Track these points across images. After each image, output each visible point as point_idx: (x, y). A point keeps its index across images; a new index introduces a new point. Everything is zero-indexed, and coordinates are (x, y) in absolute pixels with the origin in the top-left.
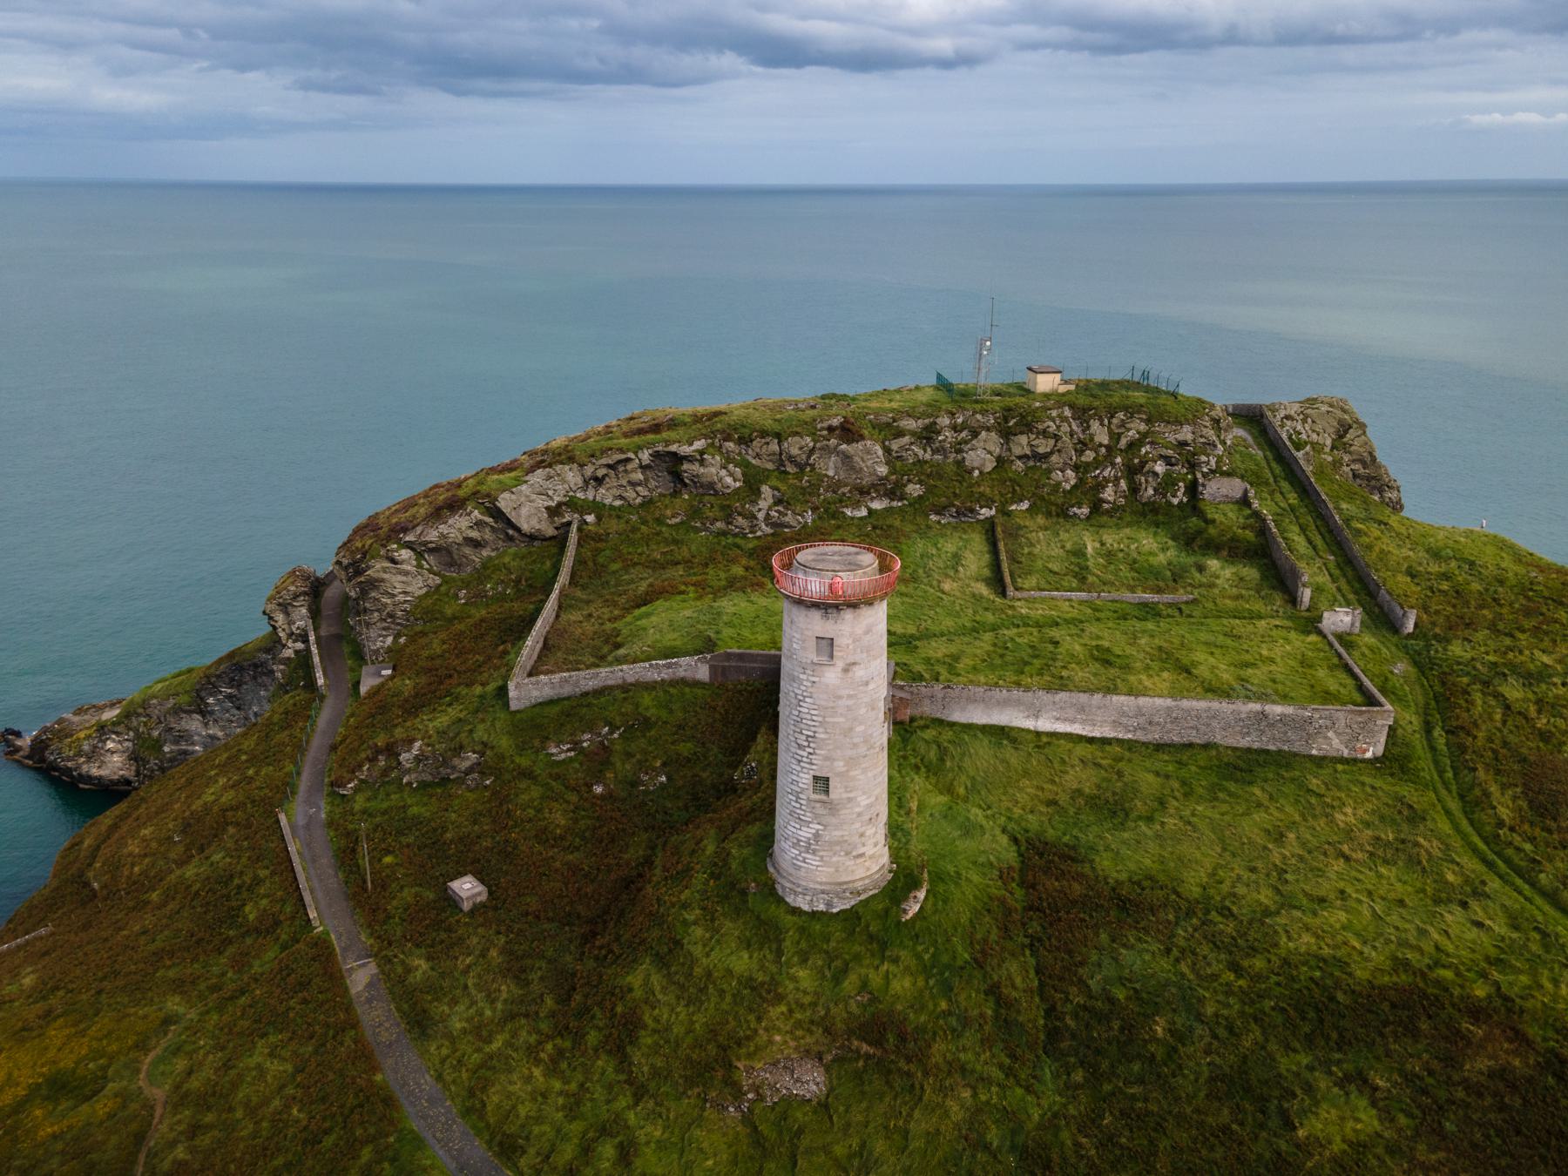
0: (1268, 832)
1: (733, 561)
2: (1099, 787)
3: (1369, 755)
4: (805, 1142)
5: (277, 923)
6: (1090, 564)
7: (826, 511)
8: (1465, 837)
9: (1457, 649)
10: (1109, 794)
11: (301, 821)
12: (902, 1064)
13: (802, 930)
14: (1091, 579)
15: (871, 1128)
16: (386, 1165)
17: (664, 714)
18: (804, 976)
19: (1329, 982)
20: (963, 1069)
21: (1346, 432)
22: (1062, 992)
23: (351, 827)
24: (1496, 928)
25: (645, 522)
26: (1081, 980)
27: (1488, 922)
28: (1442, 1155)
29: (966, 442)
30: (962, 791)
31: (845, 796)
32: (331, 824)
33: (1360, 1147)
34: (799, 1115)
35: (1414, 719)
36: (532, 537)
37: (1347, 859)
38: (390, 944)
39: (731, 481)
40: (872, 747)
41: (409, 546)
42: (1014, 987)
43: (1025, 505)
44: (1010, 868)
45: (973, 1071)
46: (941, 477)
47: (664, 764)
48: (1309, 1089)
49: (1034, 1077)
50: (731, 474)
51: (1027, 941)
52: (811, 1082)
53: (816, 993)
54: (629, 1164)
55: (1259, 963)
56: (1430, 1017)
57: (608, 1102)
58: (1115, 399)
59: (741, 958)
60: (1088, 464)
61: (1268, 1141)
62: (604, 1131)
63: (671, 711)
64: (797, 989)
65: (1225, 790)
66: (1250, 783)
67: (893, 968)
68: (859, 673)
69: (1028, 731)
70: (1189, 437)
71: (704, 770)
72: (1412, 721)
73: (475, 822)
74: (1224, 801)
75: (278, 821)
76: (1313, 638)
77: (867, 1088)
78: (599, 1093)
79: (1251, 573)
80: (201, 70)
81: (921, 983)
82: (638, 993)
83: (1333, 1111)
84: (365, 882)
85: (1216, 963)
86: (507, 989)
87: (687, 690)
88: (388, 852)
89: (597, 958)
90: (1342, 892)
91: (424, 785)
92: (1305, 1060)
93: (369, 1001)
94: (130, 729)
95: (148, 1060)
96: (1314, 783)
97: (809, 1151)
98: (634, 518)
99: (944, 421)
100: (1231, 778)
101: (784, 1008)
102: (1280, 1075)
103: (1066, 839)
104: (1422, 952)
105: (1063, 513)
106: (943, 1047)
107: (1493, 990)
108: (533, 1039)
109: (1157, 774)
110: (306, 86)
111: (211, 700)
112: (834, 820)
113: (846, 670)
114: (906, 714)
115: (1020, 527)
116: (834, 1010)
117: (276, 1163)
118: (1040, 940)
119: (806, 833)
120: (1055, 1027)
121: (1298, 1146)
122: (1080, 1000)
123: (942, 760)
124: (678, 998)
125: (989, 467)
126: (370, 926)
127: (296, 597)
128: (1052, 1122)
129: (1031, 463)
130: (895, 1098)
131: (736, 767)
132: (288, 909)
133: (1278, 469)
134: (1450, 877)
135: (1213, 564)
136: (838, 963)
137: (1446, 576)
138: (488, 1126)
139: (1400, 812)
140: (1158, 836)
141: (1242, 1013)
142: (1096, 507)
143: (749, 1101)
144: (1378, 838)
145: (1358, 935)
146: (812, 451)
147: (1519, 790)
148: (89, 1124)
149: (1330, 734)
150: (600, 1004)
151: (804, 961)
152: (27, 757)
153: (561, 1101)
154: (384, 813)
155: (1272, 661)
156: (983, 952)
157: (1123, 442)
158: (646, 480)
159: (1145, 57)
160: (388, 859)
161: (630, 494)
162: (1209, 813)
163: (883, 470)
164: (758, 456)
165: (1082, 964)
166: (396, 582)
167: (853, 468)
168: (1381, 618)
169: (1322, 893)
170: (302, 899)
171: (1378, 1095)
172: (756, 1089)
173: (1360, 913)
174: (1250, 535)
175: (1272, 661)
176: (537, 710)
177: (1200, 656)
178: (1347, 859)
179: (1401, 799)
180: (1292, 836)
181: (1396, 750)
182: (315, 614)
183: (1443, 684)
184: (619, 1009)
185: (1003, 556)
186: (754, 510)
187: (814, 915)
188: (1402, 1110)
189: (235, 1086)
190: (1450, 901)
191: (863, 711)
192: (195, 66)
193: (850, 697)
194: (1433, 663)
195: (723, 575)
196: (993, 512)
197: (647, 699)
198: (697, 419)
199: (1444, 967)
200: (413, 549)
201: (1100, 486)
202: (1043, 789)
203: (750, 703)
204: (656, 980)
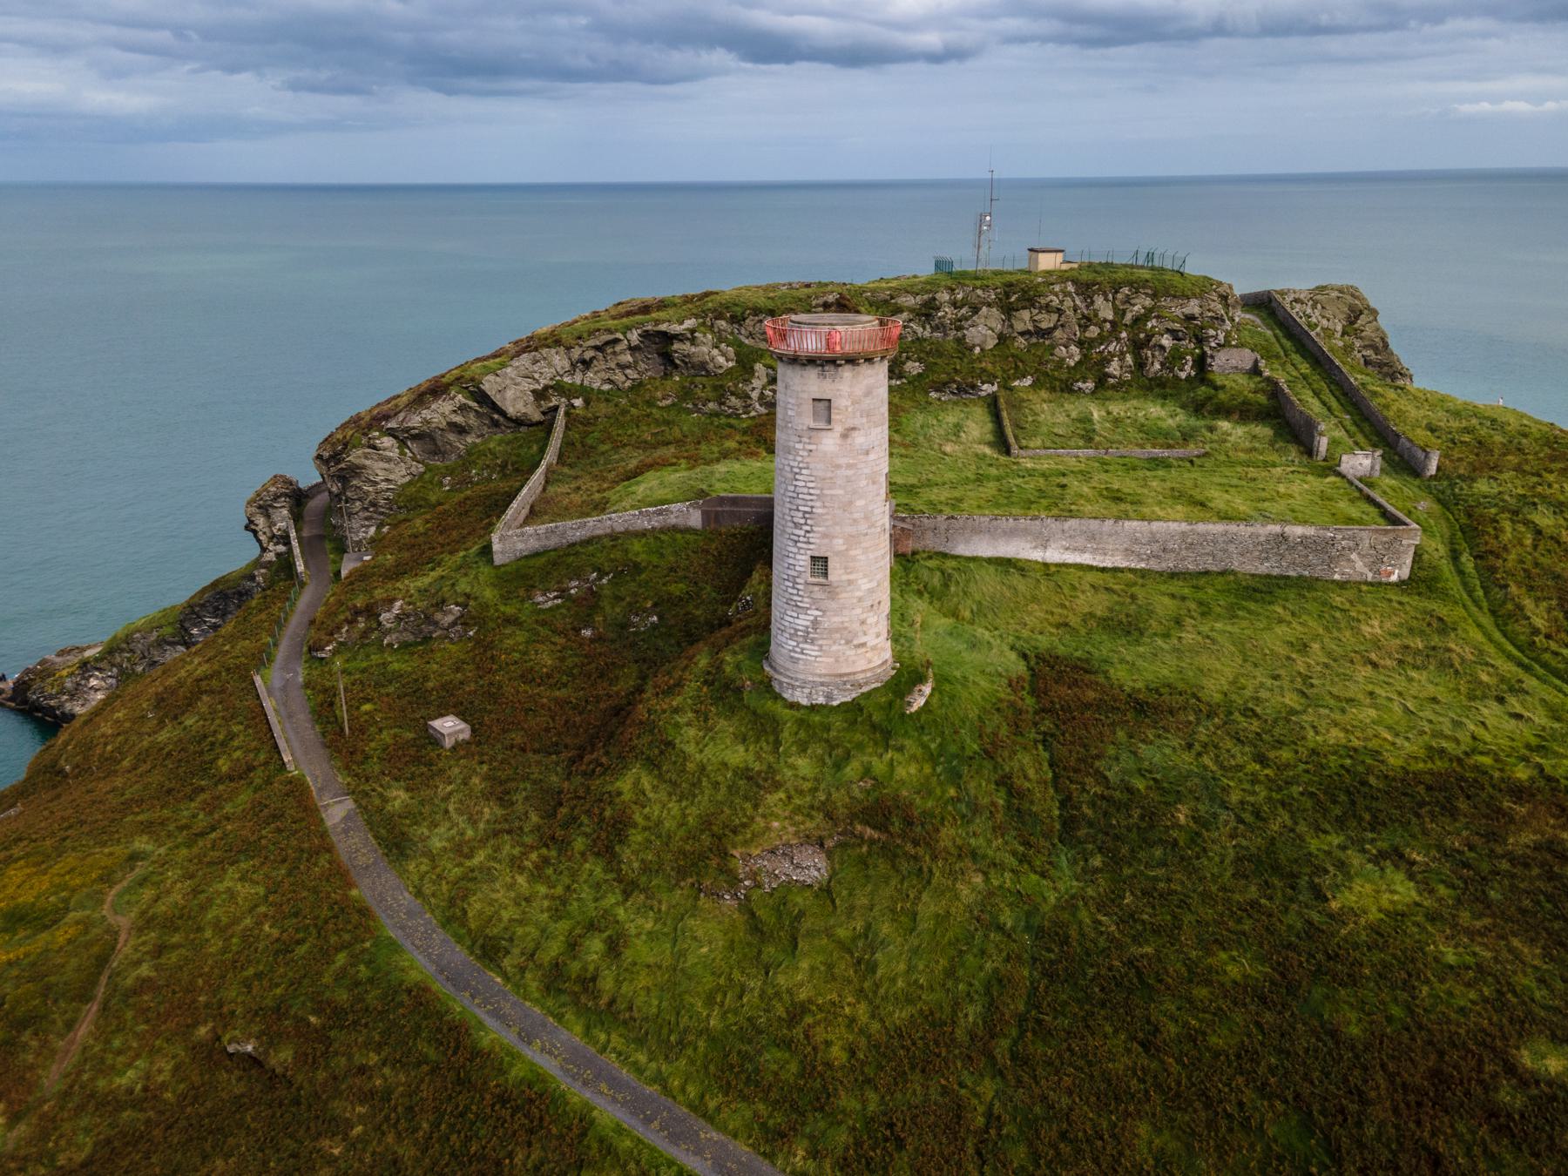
1: (727, 437)
2: (1111, 610)
3: (1394, 578)
4: (807, 924)
5: (251, 768)
6: (1097, 427)
8: (1498, 646)
9: (1482, 486)
10: (1123, 617)
11: (277, 684)
12: (909, 847)
13: (801, 722)
14: (1097, 439)
16: (362, 967)
17: (655, 559)
18: (804, 765)
19: (1361, 769)
20: (974, 855)
21: (1357, 318)
23: (328, 684)
24: (1536, 720)
25: (634, 405)
26: (1097, 771)
27: (1526, 714)
28: (1487, 921)
29: (967, 319)
30: (967, 614)
31: (845, 577)
32: (307, 685)
33: (1398, 916)
34: (799, 900)
35: (1440, 547)
36: (518, 422)
37: (1375, 665)
38: (367, 780)
39: (723, 360)
40: (872, 526)
41: (391, 433)
42: (1026, 777)
43: (1028, 381)
44: (1020, 678)
45: (984, 857)
46: (940, 355)
47: (655, 605)
48: (1342, 865)
49: (1050, 863)
50: (723, 354)
51: (1040, 737)
52: (813, 867)
53: (816, 779)
54: (618, 955)
55: (1286, 755)
56: (1468, 797)
57: (596, 900)
58: (1120, 275)
60: (1092, 340)
61: (1299, 914)
62: (592, 927)
63: (662, 556)
64: (796, 776)
65: (1244, 608)
67: (897, 756)
68: (859, 439)
69: (1037, 562)
70: (1197, 311)
71: (697, 607)
72: (1437, 550)
73: (458, 670)
74: (1244, 618)
75: (253, 683)
76: (1332, 479)
77: (871, 872)
78: (587, 893)
79: (1264, 431)
80: (194, 71)
81: (927, 769)
82: (627, 797)
83: (1368, 886)
84: (342, 729)
85: (1240, 755)
86: (489, 811)
87: (679, 536)
88: (367, 700)
89: (584, 774)
91: (405, 646)
92: (1336, 840)
93: (346, 831)
94: (113, 665)
95: (113, 892)
96: (1338, 600)
97: (810, 934)
98: (624, 401)
99: (944, 296)
100: (1250, 598)
101: (782, 795)
102: (1310, 854)
103: (1078, 654)
104: (1457, 741)
105: (1067, 388)
106: (952, 832)
107: (1535, 772)
108: (516, 851)
109: (1173, 596)
110: (295, 86)
111: (195, 631)
112: (833, 605)
113: (845, 436)
114: (909, 546)
115: (1023, 400)
116: (835, 795)
117: (245, 973)
118: (1052, 735)
119: (803, 621)
121: (1331, 916)
122: (1098, 790)
123: (946, 586)
124: (670, 794)
125: (991, 344)
126: (347, 768)
127: (276, 498)
128: (1070, 904)
129: (1034, 340)
131: (730, 605)
132: (262, 757)
133: (1288, 344)
134: (1485, 678)
135: (1224, 425)
137: (1467, 430)
138: (470, 930)
139: (1429, 625)
140: (1175, 650)
141: (1270, 799)
142: (1102, 381)
143: (746, 888)
144: (1407, 647)
145: (1389, 728)
147: (1554, 602)
148: (47, 950)
149: (1354, 556)
150: (588, 813)
152: (11, 699)
153: (546, 903)
154: (364, 671)
155: (1291, 496)
156: (993, 743)
157: (1128, 317)
158: (636, 362)
159: (1131, 50)
160: (367, 707)
161: (619, 377)
162: (1229, 628)
164: (751, 335)
165: (1098, 757)
166: (378, 469)
168: (1402, 461)
169: (1350, 694)
170: (276, 747)
172: (754, 875)
173: (1391, 710)
174: (1262, 399)
175: (1291, 496)
176: (522, 562)
177: (1214, 493)
178: (1375, 665)
180: (1316, 646)
181: (1422, 574)
182: (297, 517)
183: (1470, 516)
184: (608, 813)
185: (1006, 422)
186: (748, 389)
187: (813, 708)
188: (1443, 882)
189: (203, 908)
190: (1485, 697)
191: (863, 483)
192: (187, 67)
193: (849, 466)
194: (1457, 499)
195: (715, 449)
196: (995, 388)
197: (637, 546)
198: (688, 300)
199: (1481, 753)
200: (395, 437)
201: (1106, 361)
202: (1052, 613)
203: (744, 546)
204: (646, 782)
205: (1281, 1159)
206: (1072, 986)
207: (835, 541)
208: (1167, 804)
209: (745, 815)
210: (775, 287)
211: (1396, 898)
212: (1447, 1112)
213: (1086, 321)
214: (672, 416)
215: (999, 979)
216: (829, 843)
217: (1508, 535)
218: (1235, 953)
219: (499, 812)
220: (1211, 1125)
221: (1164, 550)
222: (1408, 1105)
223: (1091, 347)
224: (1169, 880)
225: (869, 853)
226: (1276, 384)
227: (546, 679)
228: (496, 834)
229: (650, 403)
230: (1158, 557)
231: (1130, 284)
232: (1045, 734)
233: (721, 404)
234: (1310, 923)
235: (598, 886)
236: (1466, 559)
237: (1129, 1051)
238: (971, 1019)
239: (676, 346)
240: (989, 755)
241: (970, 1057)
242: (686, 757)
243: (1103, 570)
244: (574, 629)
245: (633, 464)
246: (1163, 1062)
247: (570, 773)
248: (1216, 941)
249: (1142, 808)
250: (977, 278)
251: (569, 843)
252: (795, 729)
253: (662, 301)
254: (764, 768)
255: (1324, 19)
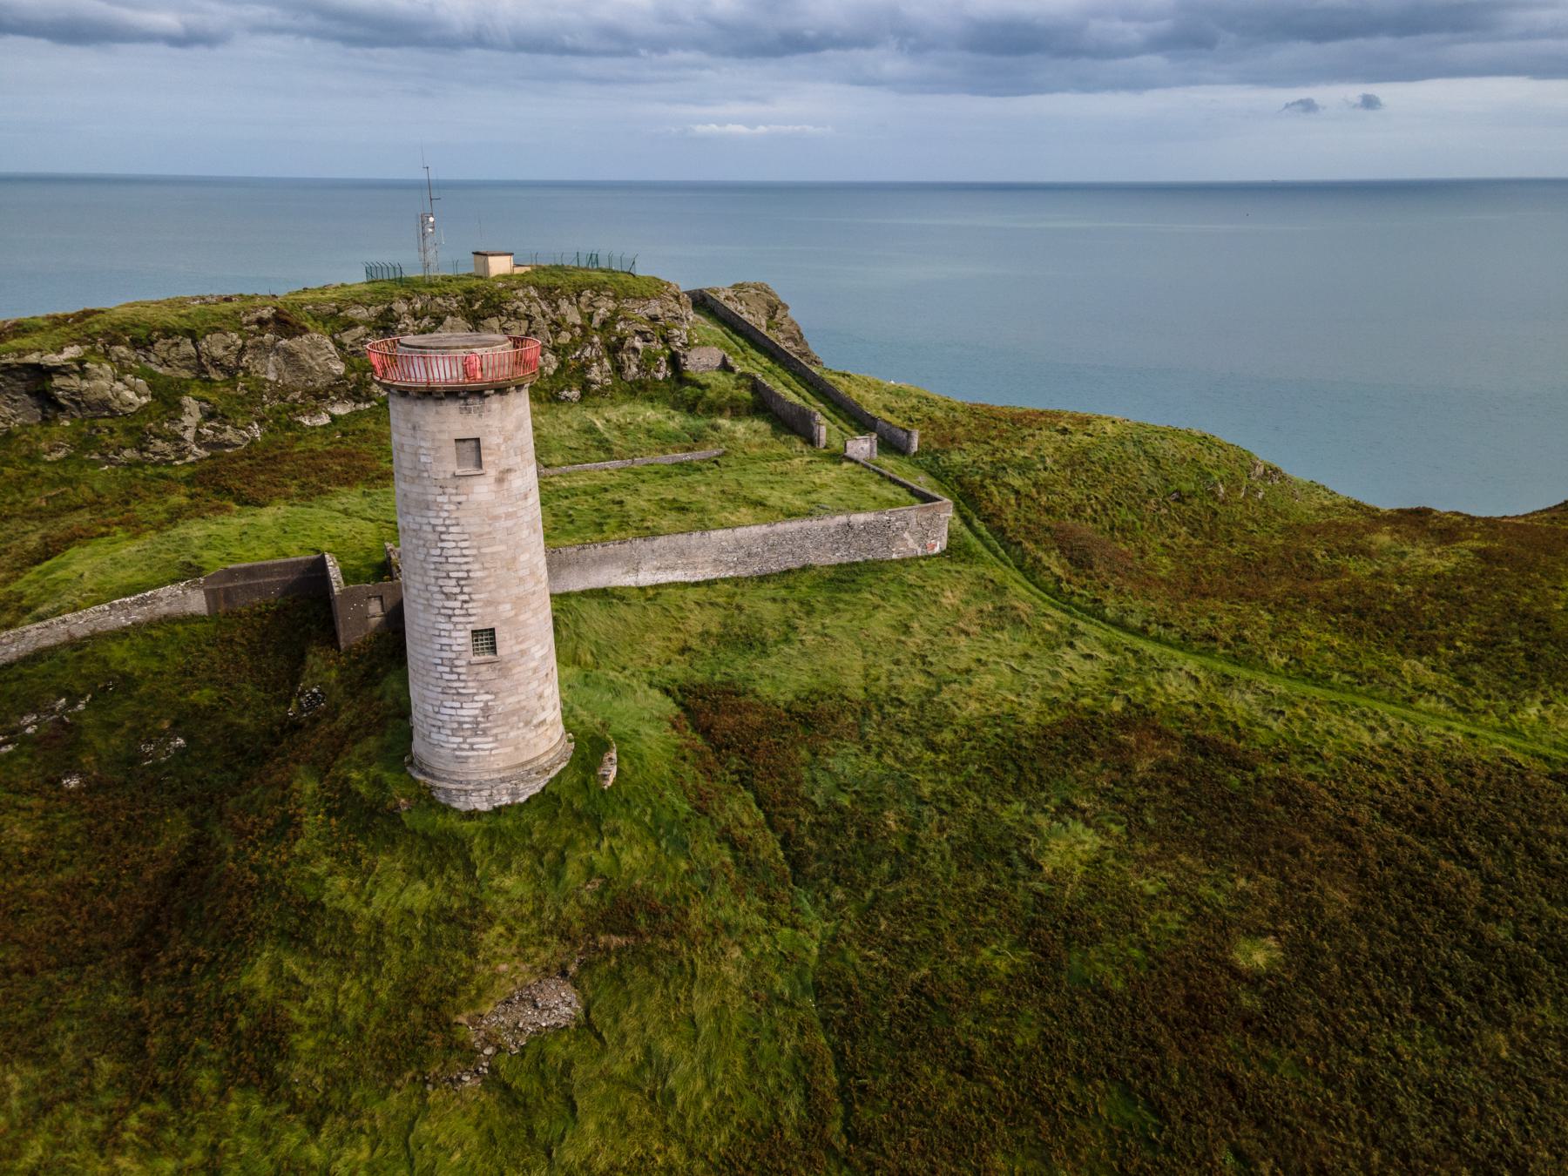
0: (893, 627)
1: (171, 492)
3: (937, 550)
4: (578, 1073)
7: (277, 422)
9: (957, 458)
10: (737, 630)
12: (663, 944)
13: (491, 833)
15: (650, 1031)
17: (154, 664)
20: (727, 927)
22: (791, 816)
26: (804, 799)
31: (516, 648)
34: (558, 1048)
39: (133, 396)
42: (742, 825)
45: (737, 927)
47: (176, 724)
48: (1034, 829)
49: (797, 911)
51: (736, 777)
52: (561, 1004)
55: (947, 736)
57: (267, 1150)
59: (418, 891)
60: (566, 346)
63: (163, 657)
64: (510, 901)
65: (841, 600)
66: (859, 591)
69: (630, 587)
70: (659, 311)
71: (241, 716)
77: (630, 986)
79: (761, 425)
81: (652, 848)
87: (179, 628)
90: (979, 660)
96: (911, 579)
99: (401, 307)
103: (718, 677)
108: (98, 1124)
109: (774, 600)
112: (506, 684)
113: (500, 480)
116: (565, 910)
119: (470, 711)
120: (799, 854)
121: (1050, 882)
122: (810, 818)
124: (339, 972)
130: (666, 985)
134: (1048, 627)
136: (549, 856)
141: (955, 783)
145: (1011, 690)
146: (242, 351)
149: (906, 535)
150: (206, 1033)
151: (506, 868)
157: (596, 322)
162: (836, 622)
163: (339, 368)
164: (165, 362)
165: (798, 782)
167: (301, 368)
169: (963, 666)
171: (1088, 815)
174: (747, 395)
178: (967, 634)
179: (981, 577)
180: (916, 625)
181: (955, 542)
184: (242, 1023)
186: (178, 428)
187: (498, 811)
188: (1112, 821)
191: (525, 533)
193: (508, 516)
198: (58, 322)
201: (585, 367)
205: (1122, 1136)
206: (869, 1032)
207: (501, 608)
208: (875, 813)
209: (461, 969)
210: (182, 303)
211: (1087, 847)
212: (1215, 1033)
213: (557, 326)
214: (71, 472)
215: (805, 1058)
216: (572, 969)
217: (997, 499)
218: (994, 947)
219: (34, 1074)
220: (1055, 1129)
221: (749, 555)
222: (1187, 1038)
223: (566, 354)
224: (909, 892)
225: (619, 964)
226: (754, 378)
227: (31, 861)
228: (46, 1108)
229: (32, 458)
230: (744, 563)
231: (591, 286)
232: (737, 772)
233: (141, 450)
234: (1038, 894)
235: (263, 1130)
236: (976, 523)
237: (952, 1084)
238: (794, 1114)
239: (58, 381)
240: (702, 811)
241: (810, 1158)
242: (349, 918)
243: (697, 584)
244: (50, 781)
245: (33, 541)
246: (988, 1083)
247: (140, 983)
248: (976, 940)
249: (857, 825)
250: (431, 286)
251: (189, 1085)
252: (486, 843)
253: (17, 324)
254: (467, 902)
255: (568, 41)
